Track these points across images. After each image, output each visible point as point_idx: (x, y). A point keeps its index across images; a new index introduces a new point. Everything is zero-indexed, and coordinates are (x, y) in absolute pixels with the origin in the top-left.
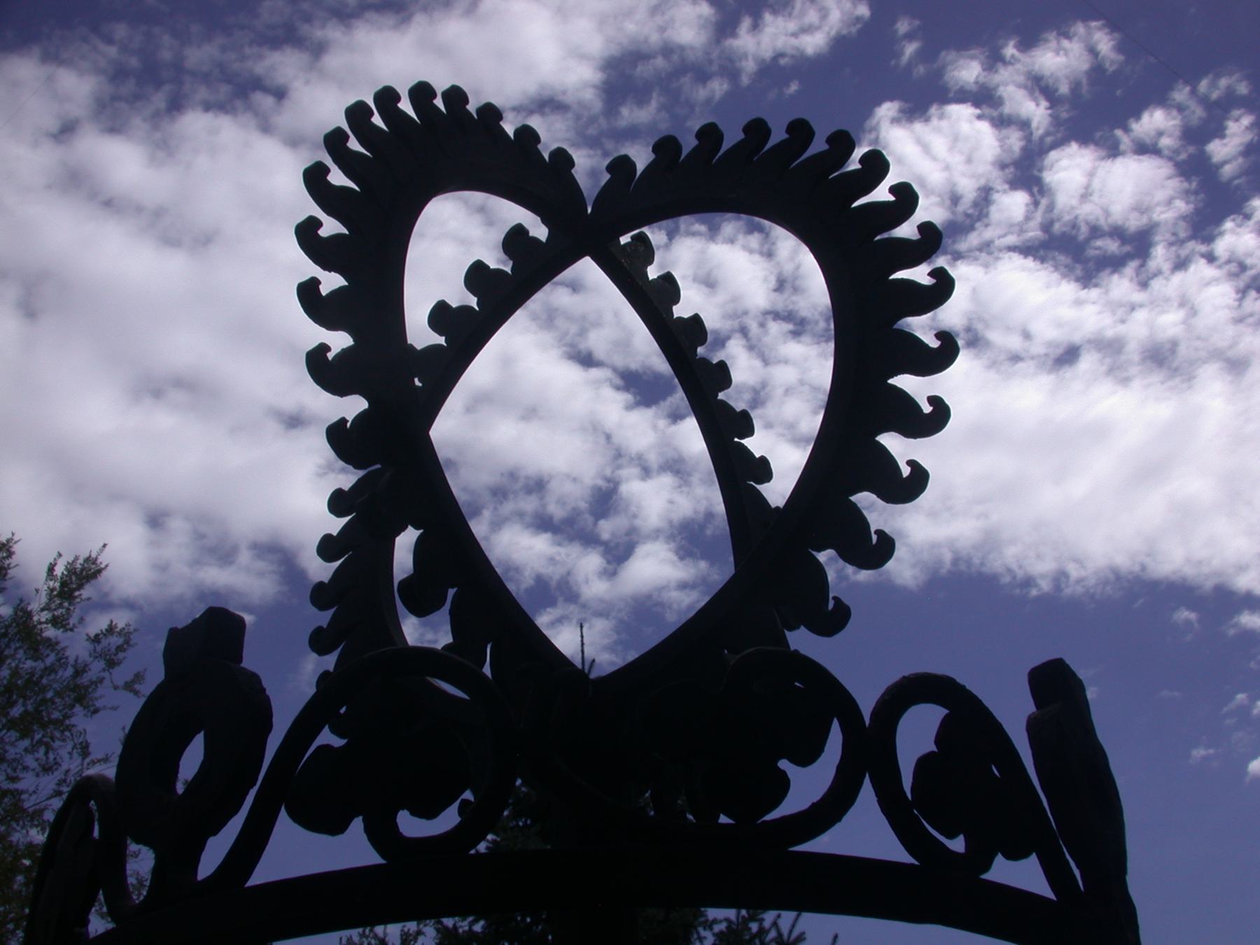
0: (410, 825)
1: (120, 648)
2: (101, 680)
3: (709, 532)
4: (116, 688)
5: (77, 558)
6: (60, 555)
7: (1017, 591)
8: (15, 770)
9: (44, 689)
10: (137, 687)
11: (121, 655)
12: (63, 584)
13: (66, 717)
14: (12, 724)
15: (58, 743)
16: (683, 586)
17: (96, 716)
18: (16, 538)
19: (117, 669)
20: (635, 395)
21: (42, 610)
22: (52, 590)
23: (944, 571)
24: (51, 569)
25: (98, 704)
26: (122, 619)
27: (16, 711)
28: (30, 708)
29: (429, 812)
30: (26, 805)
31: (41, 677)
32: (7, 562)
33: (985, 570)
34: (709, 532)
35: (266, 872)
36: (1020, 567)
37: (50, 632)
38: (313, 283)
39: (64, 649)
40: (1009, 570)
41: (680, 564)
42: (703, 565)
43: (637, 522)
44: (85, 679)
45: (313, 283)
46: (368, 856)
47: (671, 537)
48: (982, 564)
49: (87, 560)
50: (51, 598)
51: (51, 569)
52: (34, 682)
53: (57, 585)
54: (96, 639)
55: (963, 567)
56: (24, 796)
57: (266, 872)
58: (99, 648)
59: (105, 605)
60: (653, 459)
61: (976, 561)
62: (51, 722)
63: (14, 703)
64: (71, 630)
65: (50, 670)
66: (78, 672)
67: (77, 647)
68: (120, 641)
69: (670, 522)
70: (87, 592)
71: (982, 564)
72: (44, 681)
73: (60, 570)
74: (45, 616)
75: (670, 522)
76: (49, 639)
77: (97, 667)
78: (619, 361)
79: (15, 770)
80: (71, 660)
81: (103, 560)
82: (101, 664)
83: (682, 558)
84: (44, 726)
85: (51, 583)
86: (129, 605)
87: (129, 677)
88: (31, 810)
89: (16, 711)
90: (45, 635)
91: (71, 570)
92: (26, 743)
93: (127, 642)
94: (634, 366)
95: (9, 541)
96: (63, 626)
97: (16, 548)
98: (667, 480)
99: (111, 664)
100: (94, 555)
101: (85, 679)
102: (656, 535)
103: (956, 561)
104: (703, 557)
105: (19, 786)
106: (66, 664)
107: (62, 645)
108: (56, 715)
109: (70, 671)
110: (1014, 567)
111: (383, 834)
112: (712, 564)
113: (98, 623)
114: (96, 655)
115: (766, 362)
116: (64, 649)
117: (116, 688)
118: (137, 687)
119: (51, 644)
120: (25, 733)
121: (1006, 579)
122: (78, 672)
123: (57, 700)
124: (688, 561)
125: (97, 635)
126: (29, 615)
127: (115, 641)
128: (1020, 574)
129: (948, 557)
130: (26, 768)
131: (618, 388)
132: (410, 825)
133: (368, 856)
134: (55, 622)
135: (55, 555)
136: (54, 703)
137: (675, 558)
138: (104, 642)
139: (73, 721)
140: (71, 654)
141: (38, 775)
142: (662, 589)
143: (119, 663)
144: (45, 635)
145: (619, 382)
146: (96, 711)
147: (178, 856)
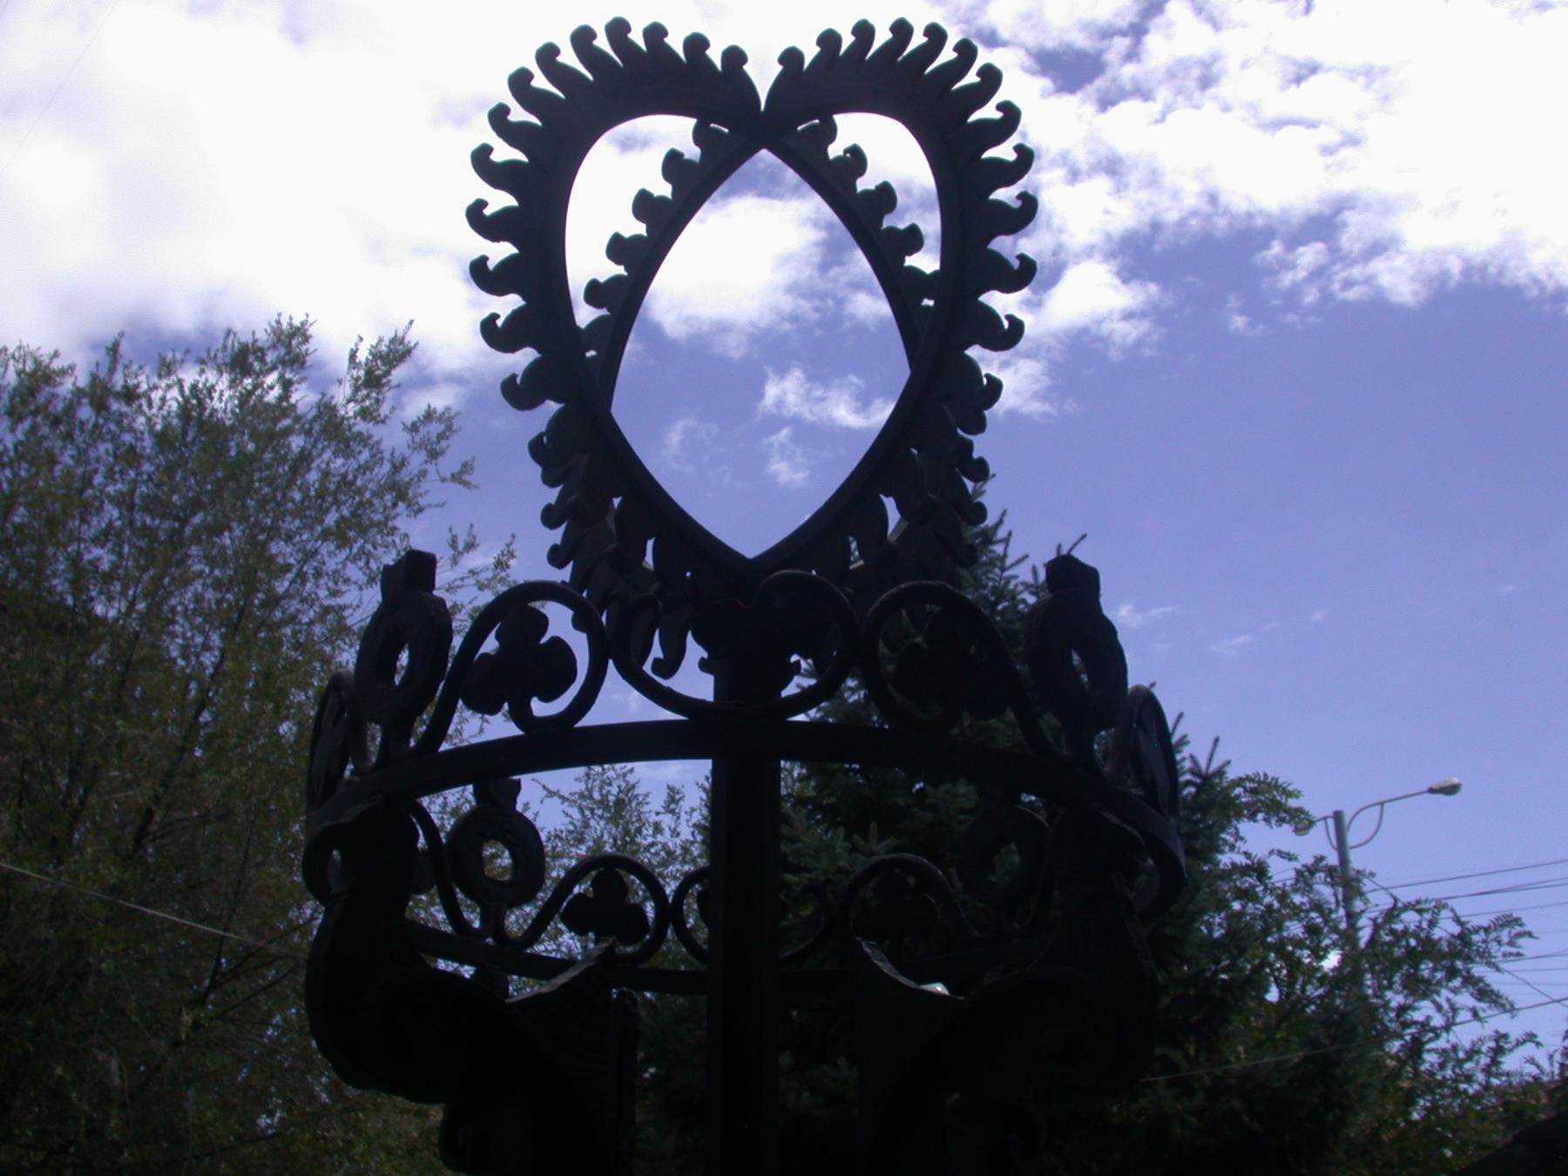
0: (539, 708)
1: (441, 436)
2: (423, 474)
3: (1157, 248)
4: (443, 480)
5: (381, 340)
6: (361, 339)
7: (1547, 307)
8: (336, 583)
9: (359, 492)
10: (466, 477)
11: (444, 444)
12: (369, 372)
13: (387, 518)
14: (326, 535)
15: (381, 550)
16: (1128, 316)
17: (420, 516)
18: (311, 320)
19: (440, 460)
20: (1055, 81)
21: (349, 401)
22: (357, 379)
23: (1452, 284)
24: (353, 355)
25: (422, 502)
26: (440, 399)
27: (331, 519)
28: (346, 512)
29: (548, 697)
30: (349, 622)
31: (355, 477)
32: (304, 348)
33: (1505, 281)
34: (1157, 248)
35: (593, 718)
36: (1550, 276)
37: (361, 426)
38: (480, 205)
39: (378, 443)
40: (1536, 281)
41: (1123, 288)
42: (1153, 288)
43: (1064, 238)
44: (404, 476)
45: (480, 205)
46: (511, 730)
47: (1110, 255)
48: (1501, 273)
49: (393, 341)
50: (357, 389)
51: (353, 355)
52: (346, 483)
53: (362, 373)
54: (414, 428)
55: (1476, 278)
56: (348, 612)
57: (593, 718)
58: (417, 439)
59: (425, 381)
60: (1081, 158)
61: (1492, 270)
62: (373, 524)
63: (327, 511)
64: (383, 422)
65: (365, 468)
66: (397, 467)
67: (392, 438)
68: (442, 428)
69: (1108, 237)
70: (398, 374)
71: (1501, 273)
72: (359, 483)
73: (363, 356)
74: (352, 408)
75: (1108, 237)
76: (360, 434)
77: (417, 460)
78: (1030, 38)
79: (336, 583)
80: (387, 455)
81: (411, 338)
82: (423, 456)
83: (1125, 281)
84: (363, 531)
85: (355, 373)
86: (453, 379)
87: (456, 469)
88: (355, 628)
89: (331, 519)
90: (355, 429)
91: (376, 355)
92: (344, 554)
93: (449, 428)
94: (1050, 45)
95: (303, 324)
96: (374, 418)
97: (312, 331)
98: (1102, 183)
99: (434, 455)
100: (400, 335)
101: (404, 476)
102: (1089, 252)
103: (1468, 271)
104: (1152, 279)
105: (340, 601)
106: (382, 459)
107: (376, 438)
108: (378, 517)
109: (387, 467)
110: (1542, 276)
111: (521, 715)
112: (1164, 288)
113: (415, 406)
114: (415, 447)
115: (1216, 25)
116: (378, 443)
117: (443, 480)
118: (466, 477)
119: (363, 439)
120: (344, 542)
121: (1534, 293)
122: (397, 467)
123: (376, 501)
124: (1135, 285)
125: (414, 424)
126: (334, 409)
127: (435, 428)
128: (1550, 285)
129: (1455, 266)
130: (347, 581)
131: (1033, 73)
132: (539, 708)
133: (511, 730)
134: (365, 414)
135: (356, 339)
136: (372, 505)
137: (1117, 282)
138: (423, 431)
139: (398, 523)
140: (386, 446)
141: (361, 588)
142: (1099, 322)
143: (442, 453)
144: (355, 429)
145: (1029, 62)
146: (421, 510)
147: (398, 729)
